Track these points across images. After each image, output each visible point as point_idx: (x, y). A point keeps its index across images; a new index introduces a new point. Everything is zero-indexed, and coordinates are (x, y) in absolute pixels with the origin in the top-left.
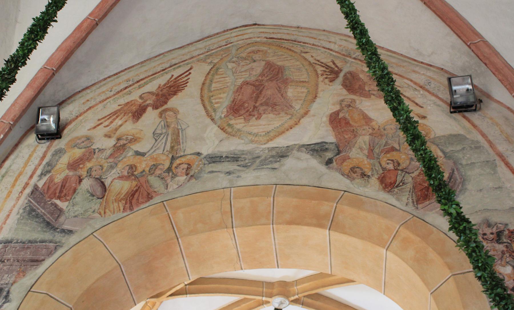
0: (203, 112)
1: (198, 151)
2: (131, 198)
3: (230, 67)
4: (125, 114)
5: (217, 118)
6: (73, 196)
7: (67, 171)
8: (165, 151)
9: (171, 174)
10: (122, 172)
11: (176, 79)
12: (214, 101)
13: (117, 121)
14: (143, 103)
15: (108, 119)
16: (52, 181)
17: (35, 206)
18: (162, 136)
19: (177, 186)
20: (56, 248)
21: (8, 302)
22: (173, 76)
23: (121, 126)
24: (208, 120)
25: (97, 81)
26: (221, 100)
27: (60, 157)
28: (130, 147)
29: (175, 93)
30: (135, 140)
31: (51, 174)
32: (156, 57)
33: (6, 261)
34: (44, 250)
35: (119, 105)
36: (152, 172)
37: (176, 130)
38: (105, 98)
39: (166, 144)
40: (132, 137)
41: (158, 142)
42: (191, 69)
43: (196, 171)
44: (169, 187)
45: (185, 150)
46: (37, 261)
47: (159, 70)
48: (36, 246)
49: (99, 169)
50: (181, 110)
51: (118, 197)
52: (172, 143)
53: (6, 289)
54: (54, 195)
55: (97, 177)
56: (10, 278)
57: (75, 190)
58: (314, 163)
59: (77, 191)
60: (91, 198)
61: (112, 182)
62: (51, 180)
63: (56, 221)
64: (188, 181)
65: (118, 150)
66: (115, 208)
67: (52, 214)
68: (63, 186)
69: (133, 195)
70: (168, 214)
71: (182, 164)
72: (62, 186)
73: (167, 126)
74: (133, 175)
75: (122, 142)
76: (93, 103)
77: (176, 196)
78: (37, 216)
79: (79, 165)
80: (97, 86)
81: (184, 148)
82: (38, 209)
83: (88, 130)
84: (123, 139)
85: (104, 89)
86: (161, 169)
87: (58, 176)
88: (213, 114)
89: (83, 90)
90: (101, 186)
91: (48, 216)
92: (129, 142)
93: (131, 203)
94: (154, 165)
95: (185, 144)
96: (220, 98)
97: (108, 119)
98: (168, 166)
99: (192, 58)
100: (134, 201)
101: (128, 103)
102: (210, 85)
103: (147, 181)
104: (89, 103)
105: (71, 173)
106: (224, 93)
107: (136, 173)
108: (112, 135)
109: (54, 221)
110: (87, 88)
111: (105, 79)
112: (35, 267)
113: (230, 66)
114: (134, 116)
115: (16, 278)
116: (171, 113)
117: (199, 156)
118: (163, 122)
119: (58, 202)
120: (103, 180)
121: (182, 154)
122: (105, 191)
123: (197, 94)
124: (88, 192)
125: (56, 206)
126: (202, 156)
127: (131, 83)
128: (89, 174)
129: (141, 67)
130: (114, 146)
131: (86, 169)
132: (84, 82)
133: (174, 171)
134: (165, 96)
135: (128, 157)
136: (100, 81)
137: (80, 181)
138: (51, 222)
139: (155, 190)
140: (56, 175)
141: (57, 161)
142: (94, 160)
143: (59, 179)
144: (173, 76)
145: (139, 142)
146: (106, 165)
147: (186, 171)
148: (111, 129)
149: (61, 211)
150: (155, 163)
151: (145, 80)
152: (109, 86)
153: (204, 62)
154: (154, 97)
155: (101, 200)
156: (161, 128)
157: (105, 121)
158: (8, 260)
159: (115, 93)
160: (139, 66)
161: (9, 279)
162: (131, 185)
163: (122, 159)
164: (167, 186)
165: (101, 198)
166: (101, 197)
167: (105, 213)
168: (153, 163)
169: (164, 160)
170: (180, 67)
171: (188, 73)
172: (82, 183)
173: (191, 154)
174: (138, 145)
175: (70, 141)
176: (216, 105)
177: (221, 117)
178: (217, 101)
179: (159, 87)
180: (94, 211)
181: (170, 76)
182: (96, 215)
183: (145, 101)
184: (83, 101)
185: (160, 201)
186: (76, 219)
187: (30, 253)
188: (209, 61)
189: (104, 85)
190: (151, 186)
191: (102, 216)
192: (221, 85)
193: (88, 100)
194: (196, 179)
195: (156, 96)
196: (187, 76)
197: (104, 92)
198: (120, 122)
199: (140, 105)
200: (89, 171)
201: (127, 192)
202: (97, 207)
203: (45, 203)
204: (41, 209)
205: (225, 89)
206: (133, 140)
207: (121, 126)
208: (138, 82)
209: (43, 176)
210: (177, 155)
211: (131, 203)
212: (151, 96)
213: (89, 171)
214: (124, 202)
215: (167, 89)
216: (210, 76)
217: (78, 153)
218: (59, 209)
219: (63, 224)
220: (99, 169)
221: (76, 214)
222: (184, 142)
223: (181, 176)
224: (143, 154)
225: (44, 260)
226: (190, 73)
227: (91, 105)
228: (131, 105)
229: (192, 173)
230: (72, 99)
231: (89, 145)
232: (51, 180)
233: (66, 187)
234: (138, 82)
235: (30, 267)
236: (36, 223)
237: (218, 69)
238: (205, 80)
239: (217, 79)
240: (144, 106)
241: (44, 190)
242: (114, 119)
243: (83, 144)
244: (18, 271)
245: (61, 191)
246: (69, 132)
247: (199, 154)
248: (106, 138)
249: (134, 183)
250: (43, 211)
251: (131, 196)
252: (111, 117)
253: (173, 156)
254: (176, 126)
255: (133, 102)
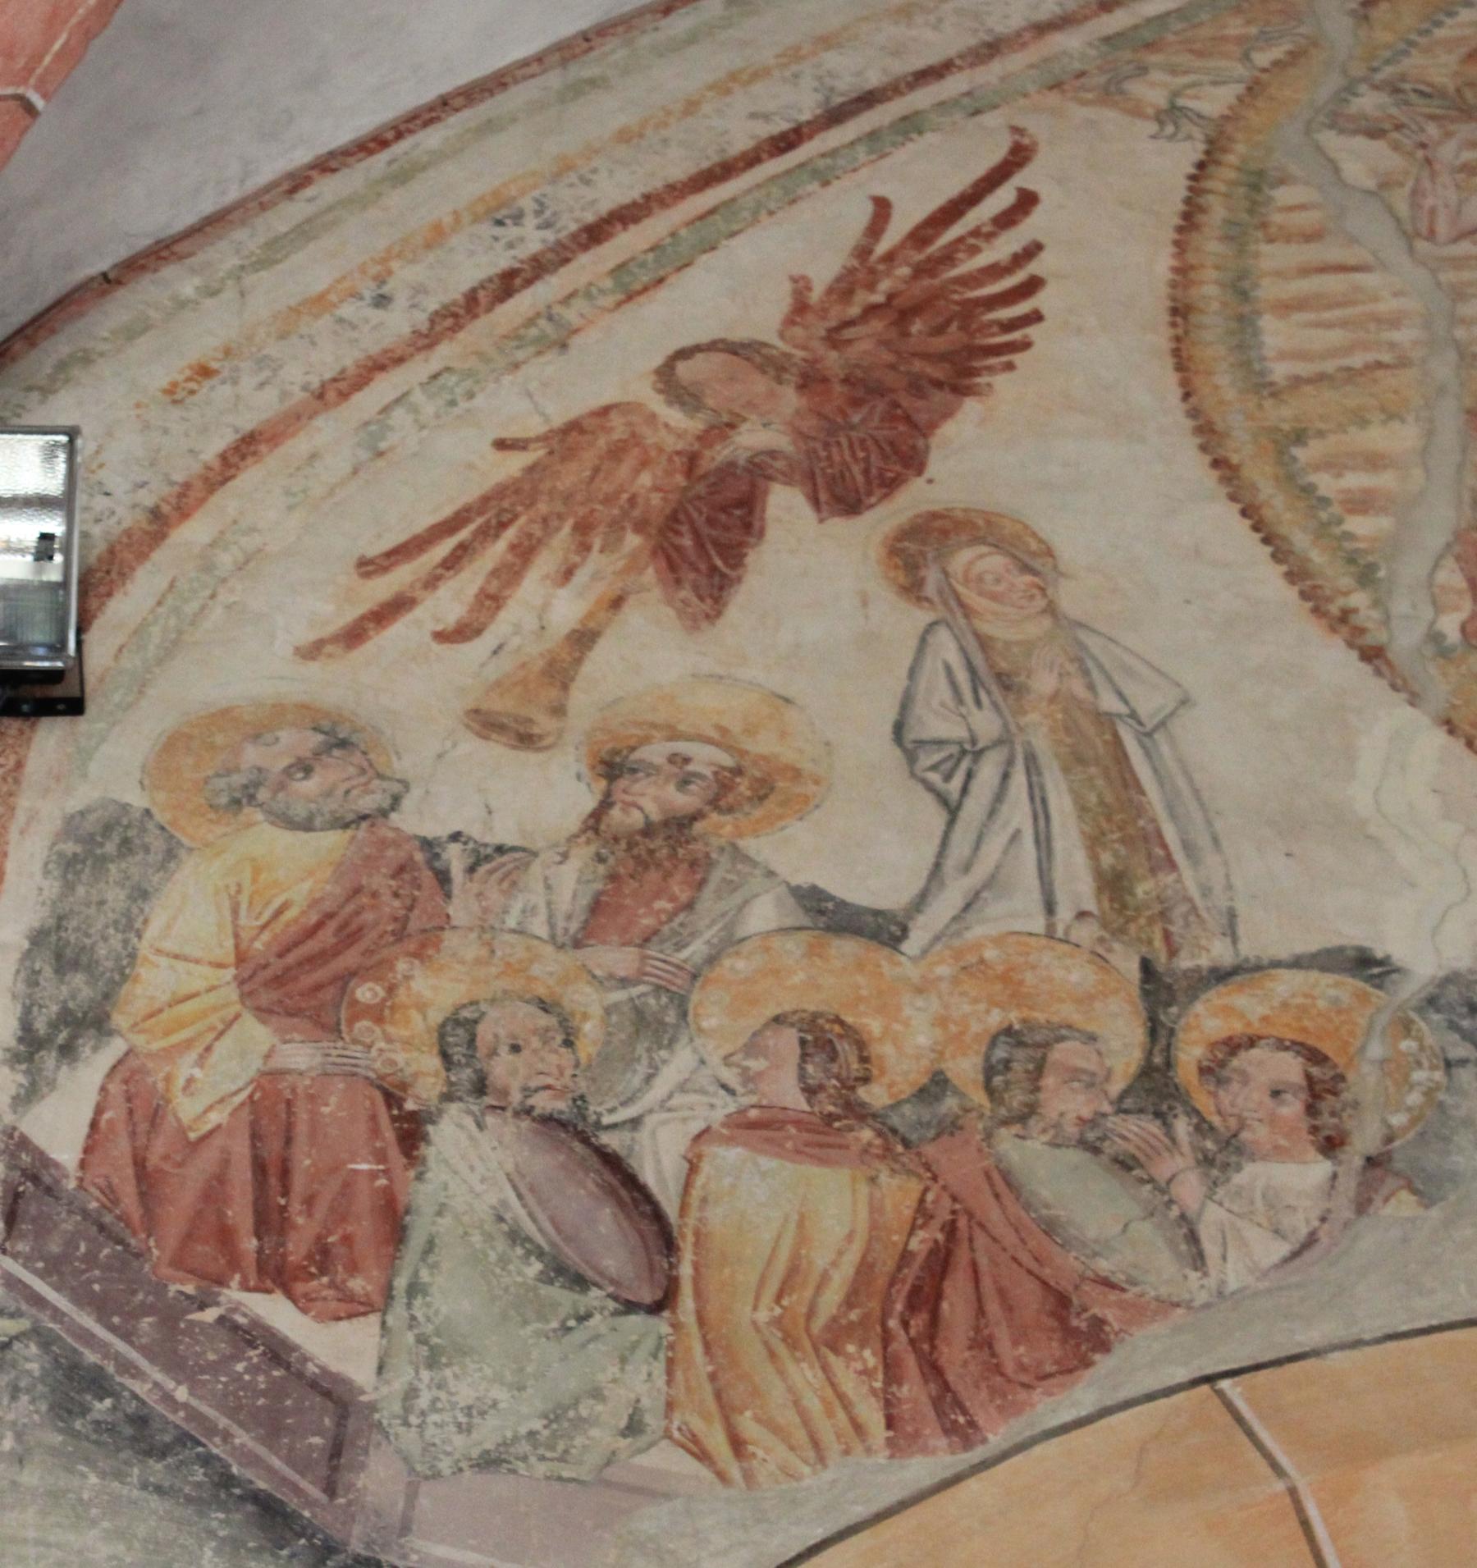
0: (1270, 582)
1: (1352, 935)
2: (918, 1323)
3: (1355, 171)
4: (583, 528)
5: (1404, 641)
6: (391, 1264)
7: (256, 1035)
8: (1064, 914)
9: (1182, 1127)
10: (748, 1078)
11: (920, 236)
12: (1325, 483)
13: (532, 586)
14: (706, 438)
15: (452, 563)
16: (155, 1117)
17: (87, 1338)
18: (988, 773)
19: (1285, 1249)
22: (882, 208)
23: (583, 639)
24: (1334, 661)
25: (233, 194)
26: (1385, 480)
27: (142, 894)
28: (738, 855)
29: (961, 374)
30: (753, 785)
31: (115, 1048)
35: (501, 445)
36: (1017, 1099)
37: (1089, 728)
38: (351, 359)
39: (1044, 843)
40: (727, 760)
41: (974, 808)
42: (1019, 156)
43: (1398, 1120)
44: (1211, 1249)
45: (1232, 915)
47: (741, 143)
49: (544, 1035)
50: (1071, 537)
51: (797, 1301)
52: (1094, 843)
54: (212, 1253)
55: (543, 1103)
57: (394, 1222)
59: (418, 1231)
60: (563, 1298)
61: (693, 1168)
62: (136, 1103)
63: (331, 1490)
64: (1362, 1206)
65: (643, 864)
66: (813, 1404)
67: (272, 1427)
68: (271, 1172)
69: (925, 1297)
70: (1293, 1492)
71: (1252, 1042)
72: (260, 1167)
73: (997, 678)
74: (859, 1113)
75: (651, 799)
76: (259, 406)
77: (1307, 1338)
78: (141, 1434)
79: (344, 980)
80: (247, 239)
81: (1223, 903)
82: (127, 1368)
83: (312, 651)
84: (651, 770)
85: (311, 271)
86: (1092, 1082)
87: (186, 1067)
88: (1358, 599)
89: (136, 266)
90: (612, 1192)
91: (242, 1438)
92: (714, 803)
93: (933, 1370)
94: (1008, 1031)
95: (1211, 859)
96: (1374, 462)
97: (452, 563)
98: (1136, 1056)
99: (992, 49)
100: (954, 1353)
101: (574, 427)
102: (1244, 324)
103: (1004, 1182)
104: (220, 392)
105: (301, 1056)
106: (1391, 415)
107: (875, 1095)
108: (544, 723)
109: (315, 1492)
110: (162, 252)
111: (296, 182)
113: (1360, 160)
114: (671, 563)
116: (995, 562)
117: (1378, 981)
118: (943, 636)
119: (276, 1312)
120: (607, 1139)
121: (1220, 952)
122: (669, 1244)
123: (1154, 391)
124: (515, 1236)
125: (278, 1351)
126: (1409, 990)
127: (533, 240)
128: (466, 1074)
129: (576, 90)
130: (595, 820)
131: (420, 1026)
132: (148, 205)
133: (1202, 1100)
134: (880, 391)
135: (755, 960)
136: (260, 201)
137: (411, 1133)
138: (293, 1503)
139: (1104, 1266)
140: (170, 1054)
141: (130, 925)
142: (460, 945)
143: (208, 1090)
144: (882, 208)
145: (801, 806)
146: (589, 1004)
147: (1311, 1110)
148: (505, 665)
149: (334, 1393)
150: (1014, 1017)
151: (656, 227)
152: (353, 244)
153: (1111, 94)
154: (790, 399)
155: (661, 1325)
156: (944, 692)
157: (432, 582)
159: (421, 319)
160: (554, 79)
162: (875, 1209)
163: (712, 960)
164: (1193, 1238)
165: (656, 1308)
166: (647, 1296)
167: (738, 1445)
168: (996, 1019)
169: (1085, 1000)
170: (910, 126)
171: (1003, 198)
172: (429, 1152)
173: (1297, 963)
174: (799, 831)
175: (173, 744)
176: (1360, 525)
177: (1435, 638)
178: (1354, 480)
179: (800, 307)
180: (633, 1427)
181: (863, 213)
182: (667, 1459)
183: (723, 428)
184: (159, 377)
185: (1182, 1375)
186: (498, 1485)
188: (1152, 92)
189: (304, 232)
190: (1050, 1228)
191: (722, 1476)
192: (1336, 337)
193: (204, 372)
194: (1427, 1199)
195: (802, 387)
196: (1007, 220)
197: (319, 303)
198: (568, 609)
199: (693, 459)
200: (457, 1037)
201: (865, 1268)
202: (642, 1383)
203: (170, 1317)
204: (158, 1376)
205: (1388, 379)
206: (743, 786)
207: (583, 639)
208: (595, 234)
209: (49, 1058)
210: (1185, 962)
211: (933, 1370)
212: (760, 384)
213: (457, 1037)
214: (870, 1358)
215: (877, 325)
216: (1210, 246)
217: (297, 866)
218: (313, 1384)
219: (405, 1529)
220: (544, 1035)
221: (488, 1434)
222: (1203, 841)
223: (1279, 1153)
224: (885, 930)
226: (1027, 201)
227: (248, 422)
228: (616, 452)
229: (1365, 1139)
230: (59, 347)
231: (367, 803)
232: (136, 1103)
233: (299, 1183)
234: (595, 234)
236: (155, 1502)
237: (1257, 182)
238: (1183, 273)
239: (1279, 274)
240: (728, 470)
241: (111, 1195)
242: (510, 573)
243: (309, 786)
245: (270, 1220)
246: (129, 662)
247: (1366, 965)
248: (496, 751)
249: (899, 1192)
250: (182, 1394)
251: (912, 1306)
252: (463, 549)
253: (1147, 967)
254: (1078, 688)
255: (618, 426)
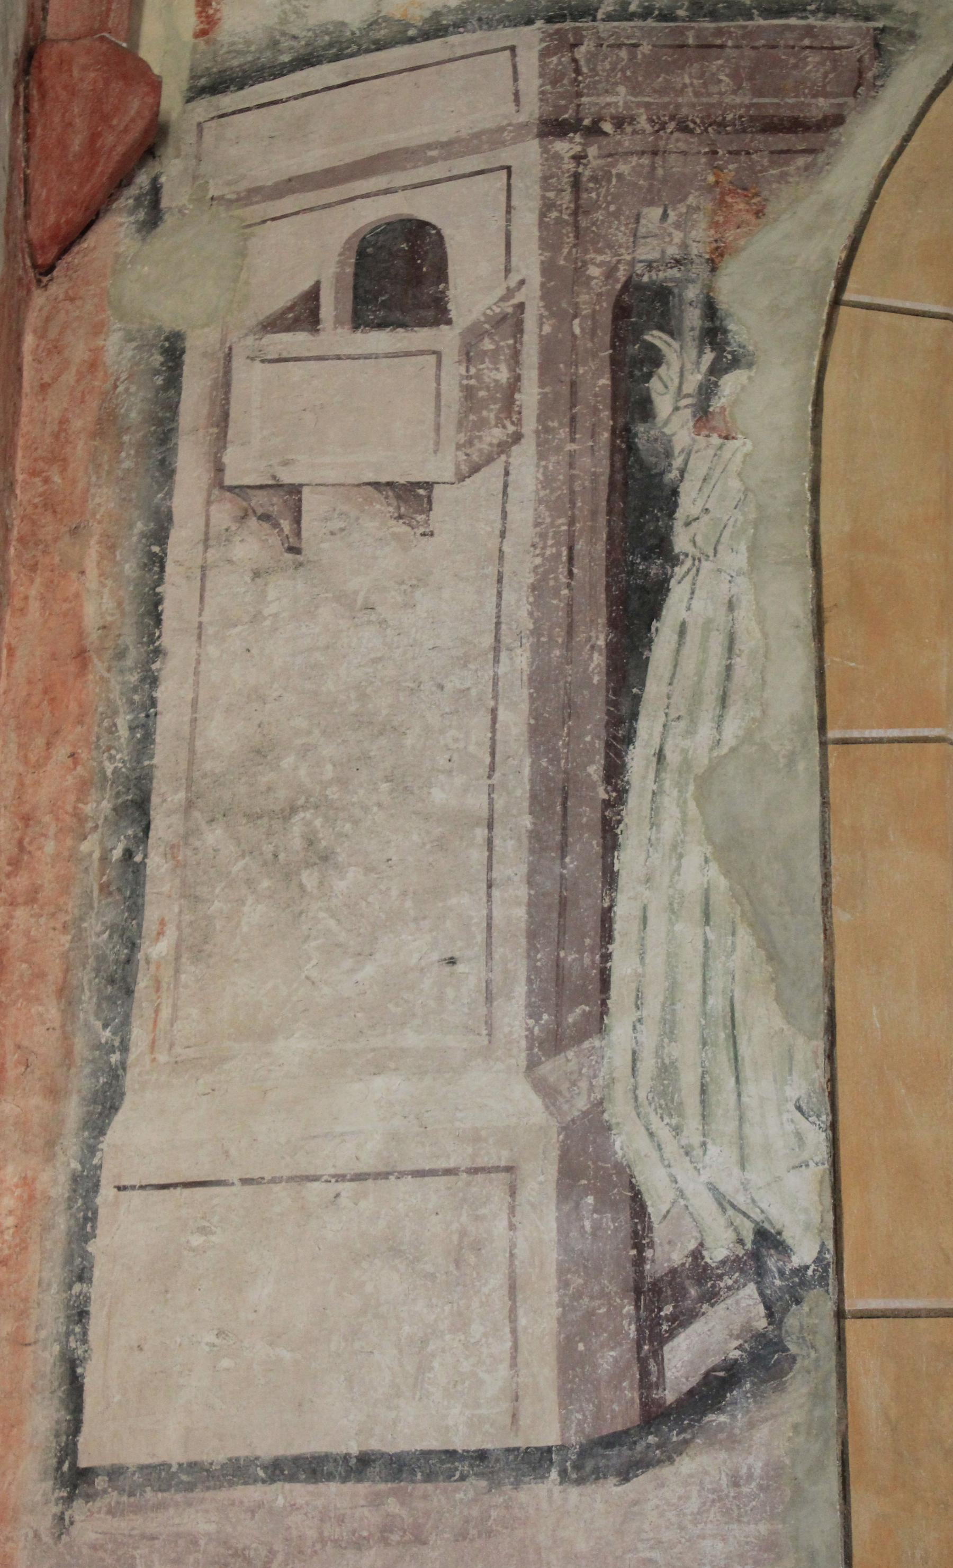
20: (877, 45)
21: (735, 363)
32: (311, 210)
33: (607, 127)
34: (813, 58)
46: (796, 125)
48: (749, 34)
53: (692, 293)
56: (677, 226)
58: (692, 1245)
112: (801, 161)
115: (715, 225)
158: (619, 123)
161: (678, 236)
187: (735, 75)
225: (838, 120)
235: (773, 164)
244: (710, 188)
